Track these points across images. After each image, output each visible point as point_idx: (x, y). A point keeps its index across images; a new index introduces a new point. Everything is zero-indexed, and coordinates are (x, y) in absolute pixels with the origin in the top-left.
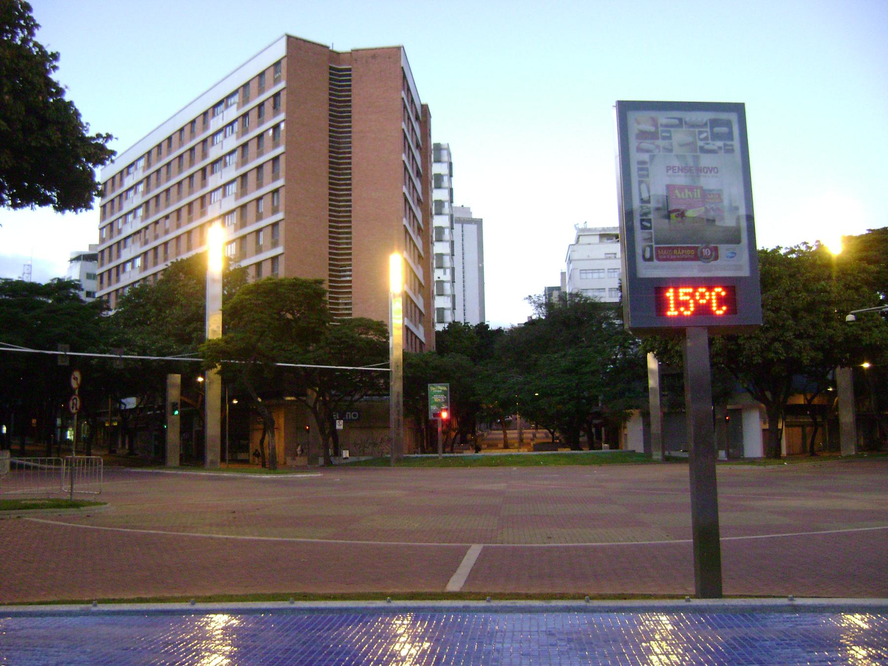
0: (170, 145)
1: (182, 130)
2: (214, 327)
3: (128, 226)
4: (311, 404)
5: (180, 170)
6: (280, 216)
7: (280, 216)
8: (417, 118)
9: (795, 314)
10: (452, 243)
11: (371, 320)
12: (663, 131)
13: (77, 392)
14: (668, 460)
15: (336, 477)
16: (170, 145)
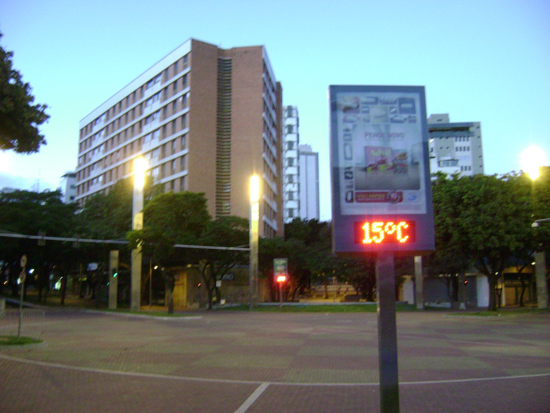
0: (120, 107)
1: (127, 97)
2: (138, 221)
3: (95, 156)
4: (201, 269)
5: (126, 123)
6: (185, 151)
7: (185, 151)
8: (273, 90)
9: (505, 218)
10: (299, 168)
11: (239, 218)
12: (363, 107)
13: (24, 269)
14: (427, 309)
15: (210, 319)
16: (120, 107)
